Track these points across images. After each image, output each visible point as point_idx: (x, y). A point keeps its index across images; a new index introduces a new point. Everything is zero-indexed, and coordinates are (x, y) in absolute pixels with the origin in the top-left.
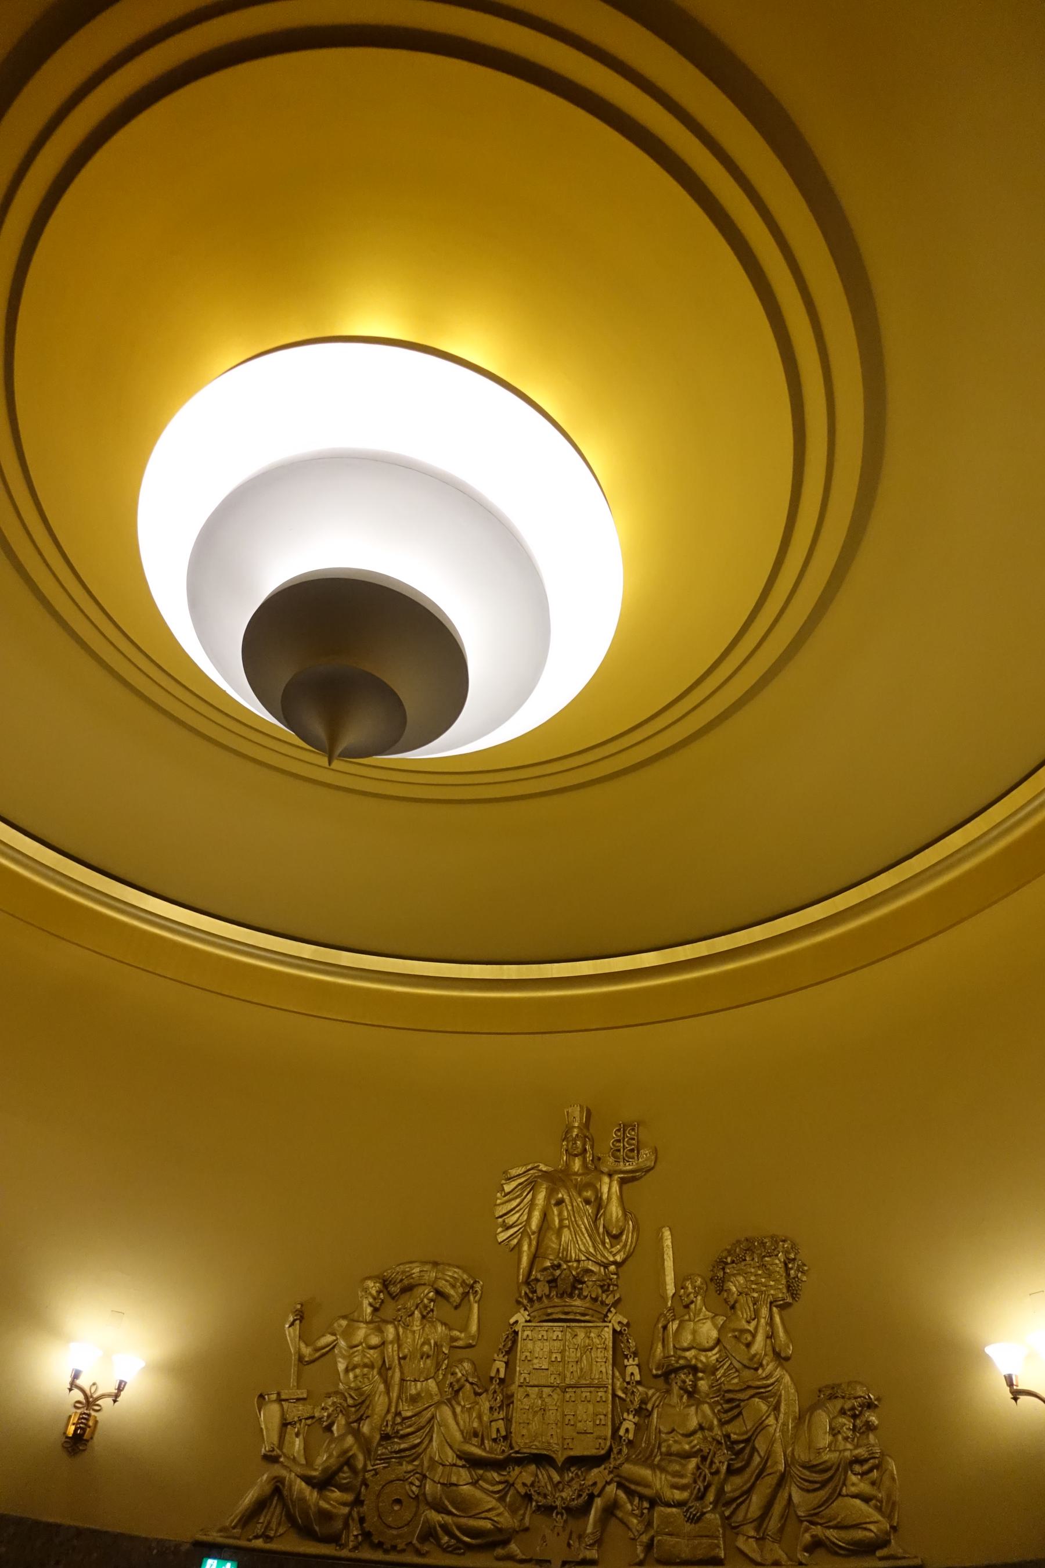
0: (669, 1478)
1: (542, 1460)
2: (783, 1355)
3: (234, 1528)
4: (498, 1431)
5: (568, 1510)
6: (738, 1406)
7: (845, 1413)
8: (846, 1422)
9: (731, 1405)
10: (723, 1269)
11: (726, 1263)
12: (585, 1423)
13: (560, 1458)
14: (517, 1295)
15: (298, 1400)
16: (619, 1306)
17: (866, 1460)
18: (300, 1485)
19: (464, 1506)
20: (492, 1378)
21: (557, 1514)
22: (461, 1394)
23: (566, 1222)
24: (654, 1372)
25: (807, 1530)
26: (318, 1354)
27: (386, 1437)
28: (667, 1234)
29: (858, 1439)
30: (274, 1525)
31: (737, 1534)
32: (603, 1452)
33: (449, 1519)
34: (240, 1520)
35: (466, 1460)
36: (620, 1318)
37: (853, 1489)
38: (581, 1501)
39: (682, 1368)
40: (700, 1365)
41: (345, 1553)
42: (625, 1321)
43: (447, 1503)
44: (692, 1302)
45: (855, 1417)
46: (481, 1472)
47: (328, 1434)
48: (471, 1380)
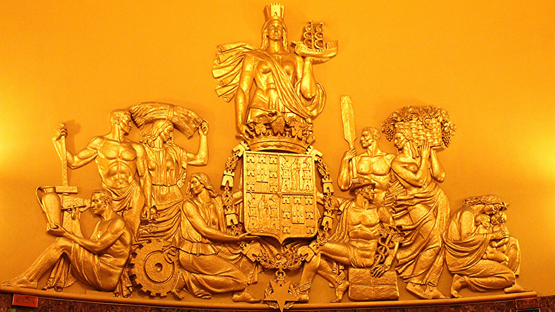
0: (359, 251)
1: (266, 240)
2: (439, 179)
3: (32, 281)
4: (232, 221)
5: (287, 271)
6: (406, 209)
7: (484, 213)
8: (487, 218)
9: (402, 207)
10: (394, 125)
11: (396, 122)
12: (300, 218)
13: (281, 239)
14: (236, 133)
15: (70, 193)
16: (314, 144)
17: (500, 240)
18: (83, 254)
19: (210, 269)
20: (222, 187)
21: (279, 273)
22: (199, 195)
23: (272, 86)
24: (343, 187)
25: (457, 279)
26: (82, 163)
27: (144, 222)
28: (345, 99)
29: (493, 228)
30: (62, 279)
31: (407, 283)
32: (313, 235)
33: (199, 276)
34: (36, 276)
35: (209, 239)
36: (316, 152)
37: (490, 255)
38: (297, 265)
39: (367, 185)
40: (377, 184)
41: (120, 298)
42: (320, 154)
43: (197, 266)
44: (370, 145)
45: (491, 215)
46: (220, 247)
47: (98, 219)
48: (208, 187)
